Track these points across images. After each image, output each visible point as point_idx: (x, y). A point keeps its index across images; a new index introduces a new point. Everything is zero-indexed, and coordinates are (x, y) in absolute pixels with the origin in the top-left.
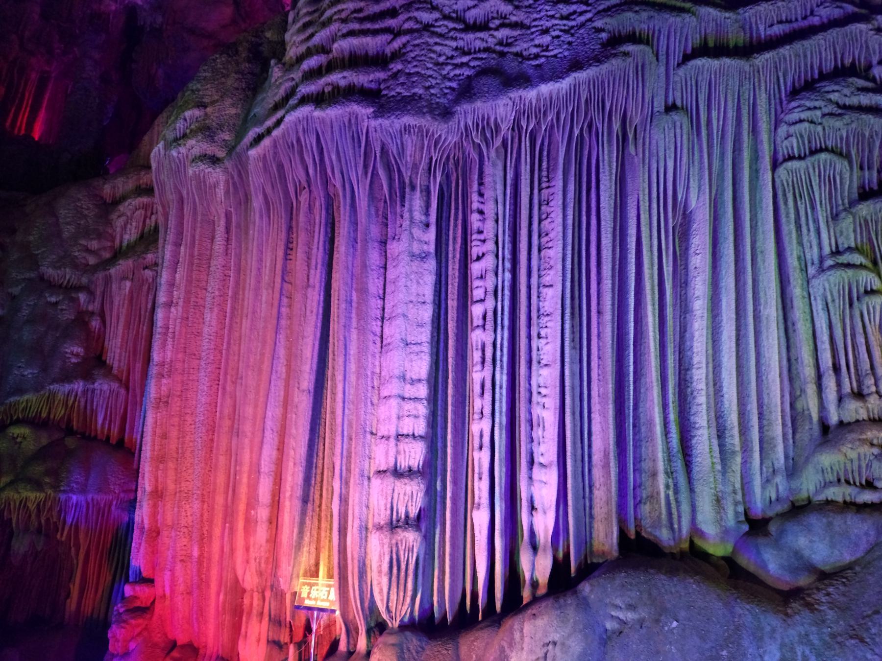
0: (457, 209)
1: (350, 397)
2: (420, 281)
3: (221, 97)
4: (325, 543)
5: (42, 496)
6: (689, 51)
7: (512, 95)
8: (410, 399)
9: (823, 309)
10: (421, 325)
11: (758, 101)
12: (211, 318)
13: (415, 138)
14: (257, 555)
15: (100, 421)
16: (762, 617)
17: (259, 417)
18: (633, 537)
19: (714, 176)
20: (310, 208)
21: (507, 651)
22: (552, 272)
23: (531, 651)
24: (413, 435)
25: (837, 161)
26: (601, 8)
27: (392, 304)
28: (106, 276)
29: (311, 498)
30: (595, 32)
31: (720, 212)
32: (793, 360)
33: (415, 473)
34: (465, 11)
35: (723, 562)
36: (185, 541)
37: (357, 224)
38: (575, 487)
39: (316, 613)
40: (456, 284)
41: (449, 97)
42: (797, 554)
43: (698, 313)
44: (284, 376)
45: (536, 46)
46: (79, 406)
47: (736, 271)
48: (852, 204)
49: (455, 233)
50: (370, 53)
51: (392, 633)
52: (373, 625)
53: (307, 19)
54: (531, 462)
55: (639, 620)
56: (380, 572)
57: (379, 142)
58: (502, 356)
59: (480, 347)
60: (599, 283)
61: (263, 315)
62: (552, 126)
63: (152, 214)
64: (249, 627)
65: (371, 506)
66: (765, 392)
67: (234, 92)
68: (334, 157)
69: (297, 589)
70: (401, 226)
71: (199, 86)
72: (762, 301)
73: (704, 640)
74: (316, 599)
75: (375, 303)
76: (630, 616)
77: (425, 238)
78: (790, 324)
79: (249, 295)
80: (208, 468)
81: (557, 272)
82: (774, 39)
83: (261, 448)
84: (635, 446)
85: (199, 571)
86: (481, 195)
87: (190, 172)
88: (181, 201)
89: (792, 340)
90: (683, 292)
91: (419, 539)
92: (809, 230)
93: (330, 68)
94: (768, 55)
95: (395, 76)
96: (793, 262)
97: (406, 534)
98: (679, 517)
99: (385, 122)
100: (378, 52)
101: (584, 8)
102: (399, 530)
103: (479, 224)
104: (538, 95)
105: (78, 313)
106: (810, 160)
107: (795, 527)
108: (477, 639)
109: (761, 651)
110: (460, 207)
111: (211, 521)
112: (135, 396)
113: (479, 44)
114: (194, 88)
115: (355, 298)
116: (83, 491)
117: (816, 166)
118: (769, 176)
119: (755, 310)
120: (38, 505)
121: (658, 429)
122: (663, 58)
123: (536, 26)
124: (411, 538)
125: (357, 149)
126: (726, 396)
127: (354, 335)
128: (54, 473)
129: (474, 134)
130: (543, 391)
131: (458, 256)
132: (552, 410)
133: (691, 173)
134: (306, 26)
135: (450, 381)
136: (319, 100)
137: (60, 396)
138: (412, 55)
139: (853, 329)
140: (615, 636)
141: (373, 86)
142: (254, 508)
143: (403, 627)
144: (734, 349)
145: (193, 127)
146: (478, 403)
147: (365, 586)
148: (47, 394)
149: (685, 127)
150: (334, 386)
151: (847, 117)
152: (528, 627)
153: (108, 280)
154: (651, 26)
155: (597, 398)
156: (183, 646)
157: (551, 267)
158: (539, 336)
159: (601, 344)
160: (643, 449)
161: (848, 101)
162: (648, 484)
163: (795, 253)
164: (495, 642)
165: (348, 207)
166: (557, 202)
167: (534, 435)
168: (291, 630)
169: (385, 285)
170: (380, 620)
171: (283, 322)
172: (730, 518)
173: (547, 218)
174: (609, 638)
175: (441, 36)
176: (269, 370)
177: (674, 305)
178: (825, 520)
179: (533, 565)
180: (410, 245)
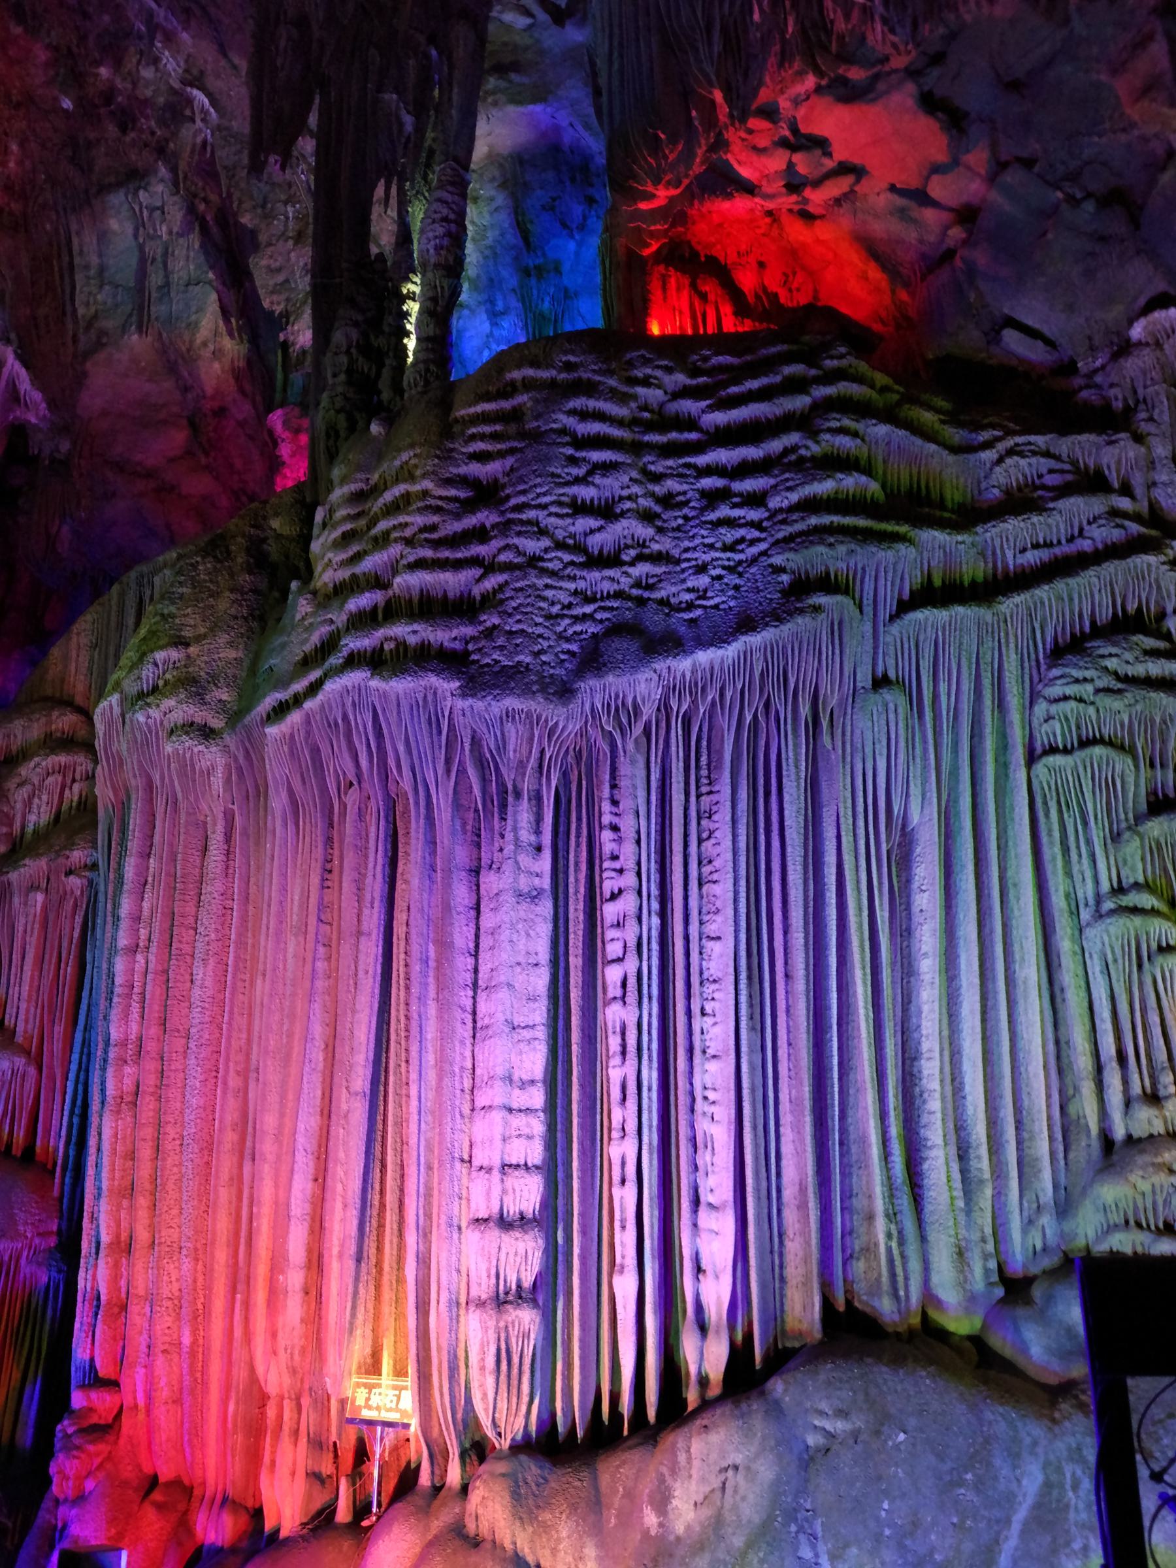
0: (579, 819)
1: (428, 1104)
3: (212, 630)
4: (388, 1322)
6: (906, 595)
7: (657, 666)
10: (532, 999)
11: (1006, 665)
16: (1019, 1424)
18: (842, 1309)
22: (719, 918)
23: (703, 1480)
26: (780, 535)
27: (489, 966)
30: (773, 573)
33: (530, 1221)
34: (586, 535)
35: (968, 1344)
36: (168, 1321)
38: (759, 1238)
39: (379, 1429)
40: (581, 933)
41: (567, 665)
43: (927, 978)
45: (689, 590)
47: (979, 912)
48: (1139, 819)
49: (577, 855)
52: (467, 1445)
53: (348, 526)
54: (696, 1202)
56: (482, 1368)
58: (650, 1041)
60: (786, 932)
61: (289, 974)
63: (74, 781)
66: (1025, 1090)
68: (401, 748)
69: (349, 1394)
70: (501, 850)
71: (173, 609)
72: (1017, 957)
73: (942, 1460)
74: (378, 1408)
76: (839, 1426)
77: (536, 868)
80: (203, 1208)
81: (727, 919)
82: (1028, 570)
83: (291, 1180)
85: (192, 1370)
86: (615, 803)
87: (169, 749)
89: (1060, 1014)
91: (538, 1320)
92: (1080, 856)
93: (391, 612)
94: (1017, 599)
95: (490, 633)
96: (1058, 902)
97: (519, 1312)
98: (906, 1278)
99: (479, 705)
101: (756, 534)
102: (509, 1307)
103: (613, 846)
104: (694, 665)
106: (1080, 755)
108: (624, 1462)
109: (1018, 1472)
110: (584, 820)
111: (208, 1288)
113: (607, 586)
114: (166, 611)
118: (1022, 775)
121: (875, 1151)
122: (869, 610)
123: (688, 560)
124: (526, 1318)
125: (435, 739)
126: (969, 1098)
130: (712, 1095)
131: (582, 890)
134: (347, 538)
136: (375, 661)
139: (1143, 1001)
140: (819, 1455)
141: (457, 645)
142: (282, 1272)
144: (978, 1029)
145: (168, 676)
146: (617, 1115)
149: (901, 710)
151: (1128, 695)
152: (697, 1446)
154: (852, 565)
156: (170, 1484)
158: (703, 1014)
160: (855, 1179)
161: (1131, 671)
162: (863, 1230)
163: (1061, 888)
164: (651, 1468)
165: (422, 821)
166: (724, 815)
167: (700, 1162)
168: (336, 1456)
169: (477, 936)
170: (477, 1438)
173: (709, 837)
174: (812, 1459)
175: (553, 574)
177: (893, 964)
179: (702, 1354)
180: (516, 880)
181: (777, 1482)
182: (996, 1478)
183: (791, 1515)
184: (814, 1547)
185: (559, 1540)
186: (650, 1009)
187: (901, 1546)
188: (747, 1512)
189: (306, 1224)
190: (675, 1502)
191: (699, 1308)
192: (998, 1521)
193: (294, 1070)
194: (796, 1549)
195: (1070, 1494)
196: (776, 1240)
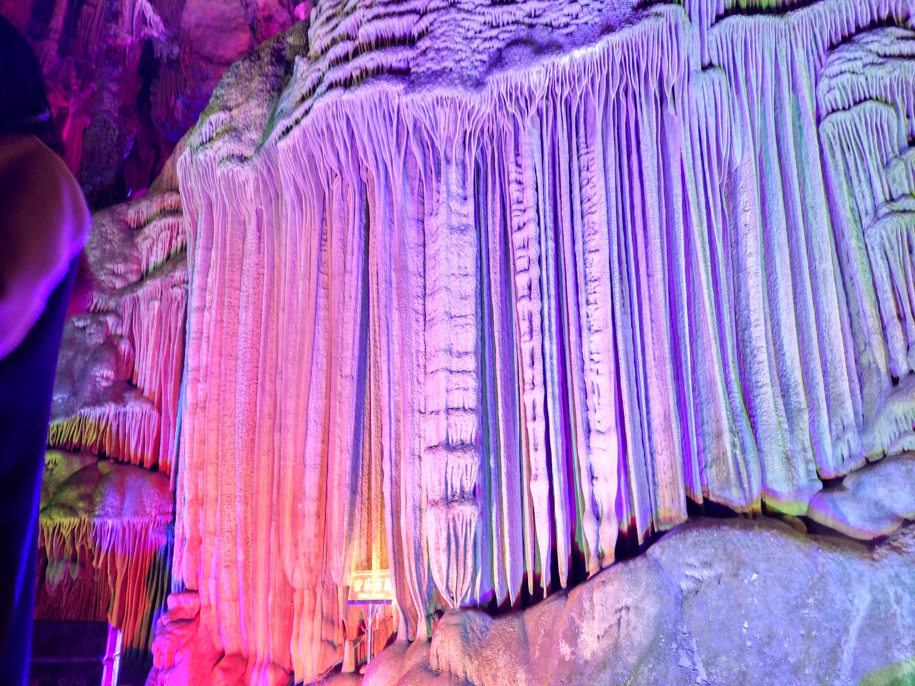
0: (494, 183)
1: (395, 378)
2: (461, 253)
4: (376, 533)
5: (76, 521)
6: (722, 11)
7: (545, 63)
8: (458, 372)
9: (882, 258)
12: (246, 316)
13: (447, 110)
14: (306, 550)
15: (133, 445)
16: (847, 564)
17: (301, 411)
19: (757, 133)
20: (343, 196)
21: (578, 621)
22: (597, 237)
23: (603, 619)
24: (464, 408)
25: (883, 109)
27: (433, 278)
28: (134, 298)
29: (359, 490)
31: (766, 170)
32: (854, 315)
35: (798, 520)
36: (229, 546)
37: (393, 205)
39: (370, 606)
40: (498, 258)
42: (878, 505)
44: (325, 367)
45: (565, 15)
46: (111, 430)
48: (902, 151)
50: (397, 35)
51: (453, 613)
52: (432, 611)
53: (331, 12)
54: (588, 431)
55: (716, 577)
56: (438, 549)
57: (412, 118)
58: (550, 326)
59: (526, 317)
62: (587, 94)
64: (301, 625)
65: (424, 486)
66: (828, 348)
67: (260, 93)
68: (366, 138)
69: (349, 584)
70: (438, 201)
71: (223, 91)
72: (817, 257)
73: (788, 590)
74: (370, 592)
75: (415, 282)
76: (706, 573)
77: (464, 211)
78: (847, 279)
79: (285, 289)
80: (250, 470)
83: (305, 440)
84: (696, 411)
86: (518, 165)
87: (218, 173)
88: (210, 205)
90: (734, 252)
91: (476, 514)
92: (860, 181)
93: (356, 53)
95: (424, 53)
97: (462, 507)
98: (749, 476)
100: (405, 34)
102: (455, 504)
104: (571, 60)
105: (107, 337)
106: (856, 110)
107: (872, 479)
109: (850, 596)
111: (255, 523)
112: (167, 417)
113: (507, 18)
115: (394, 278)
116: (119, 514)
117: (862, 115)
119: (810, 266)
120: (73, 530)
121: (720, 387)
122: (695, 17)
124: (468, 511)
126: (787, 354)
127: (396, 315)
128: (88, 498)
129: (508, 103)
130: (596, 357)
131: (498, 229)
132: (607, 375)
133: (733, 130)
134: (329, 19)
135: (498, 355)
136: (347, 84)
137: (91, 421)
138: (440, 31)
140: (691, 595)
141: (402, 65)
142: (301, 502)
143: (464, 608)
144: (792, 305)
145: (219, 130)
146: (528, 374)
147: (422, 569)
148: (78, 419)
150: (379, 371)
153: (136, 302)
155: (653, 362)
156: (231, 656)
157: (596, 232)
159: (653, 307)
162: (713, 446)
163: (847, 204)
165: (382, 188)
171: (322, 313)
172: (803, 480)
175: (468, 11)
176: (310, 360)
177: (727, 265)
178: (903, 468)
181: (660, 615)
182: (833, 600)
183: (672, 637)
184: (691, 658)
185: (498, 669)
186: (549, 304)
187: (761, 653)
188: (638, 638)
189: (318, 471)
190: (583, 637)
191: (594, 504)
192: (838, 631)
193: (305, 367)
194: (678, 660)
195: (895, 606)
196: (649, 456)
